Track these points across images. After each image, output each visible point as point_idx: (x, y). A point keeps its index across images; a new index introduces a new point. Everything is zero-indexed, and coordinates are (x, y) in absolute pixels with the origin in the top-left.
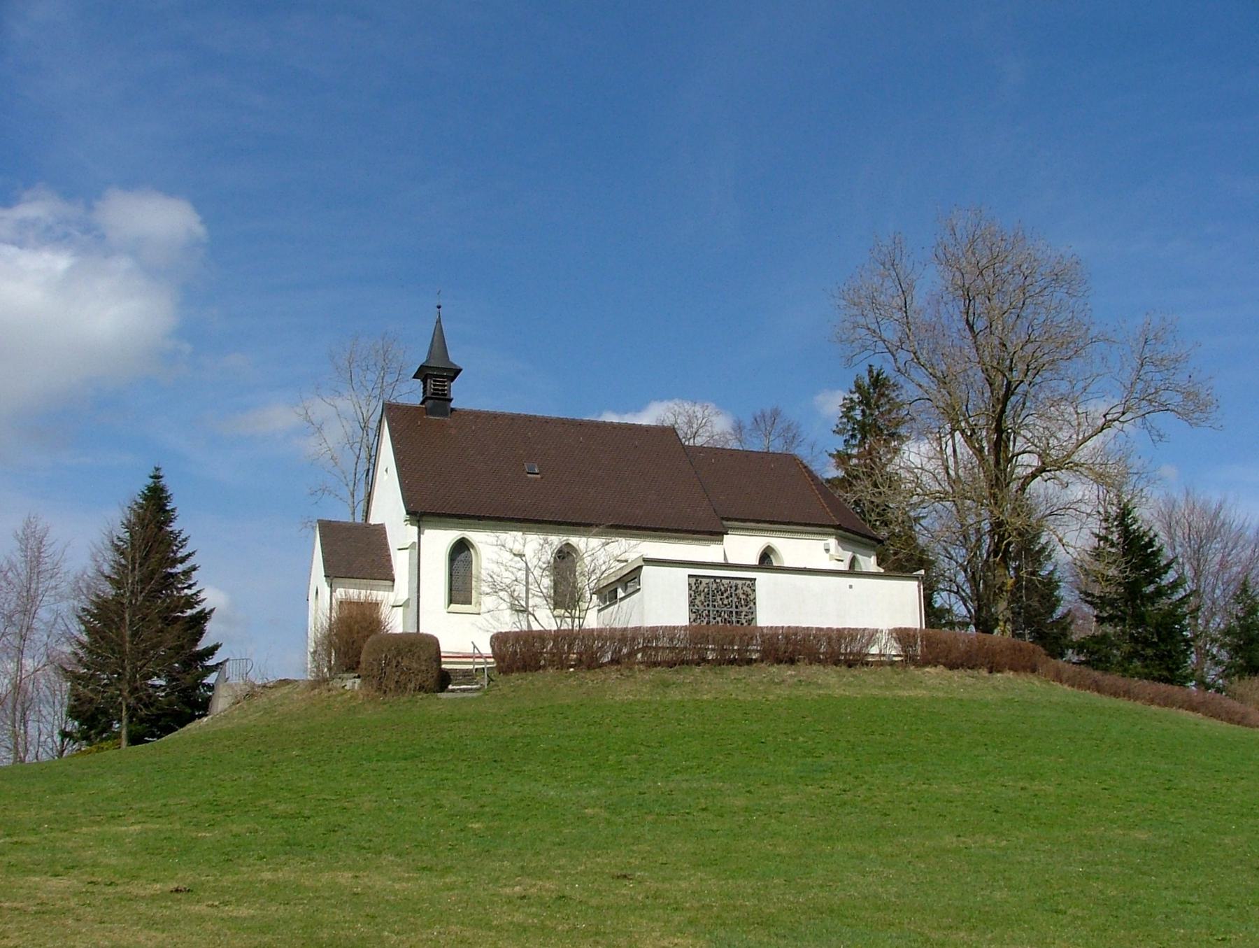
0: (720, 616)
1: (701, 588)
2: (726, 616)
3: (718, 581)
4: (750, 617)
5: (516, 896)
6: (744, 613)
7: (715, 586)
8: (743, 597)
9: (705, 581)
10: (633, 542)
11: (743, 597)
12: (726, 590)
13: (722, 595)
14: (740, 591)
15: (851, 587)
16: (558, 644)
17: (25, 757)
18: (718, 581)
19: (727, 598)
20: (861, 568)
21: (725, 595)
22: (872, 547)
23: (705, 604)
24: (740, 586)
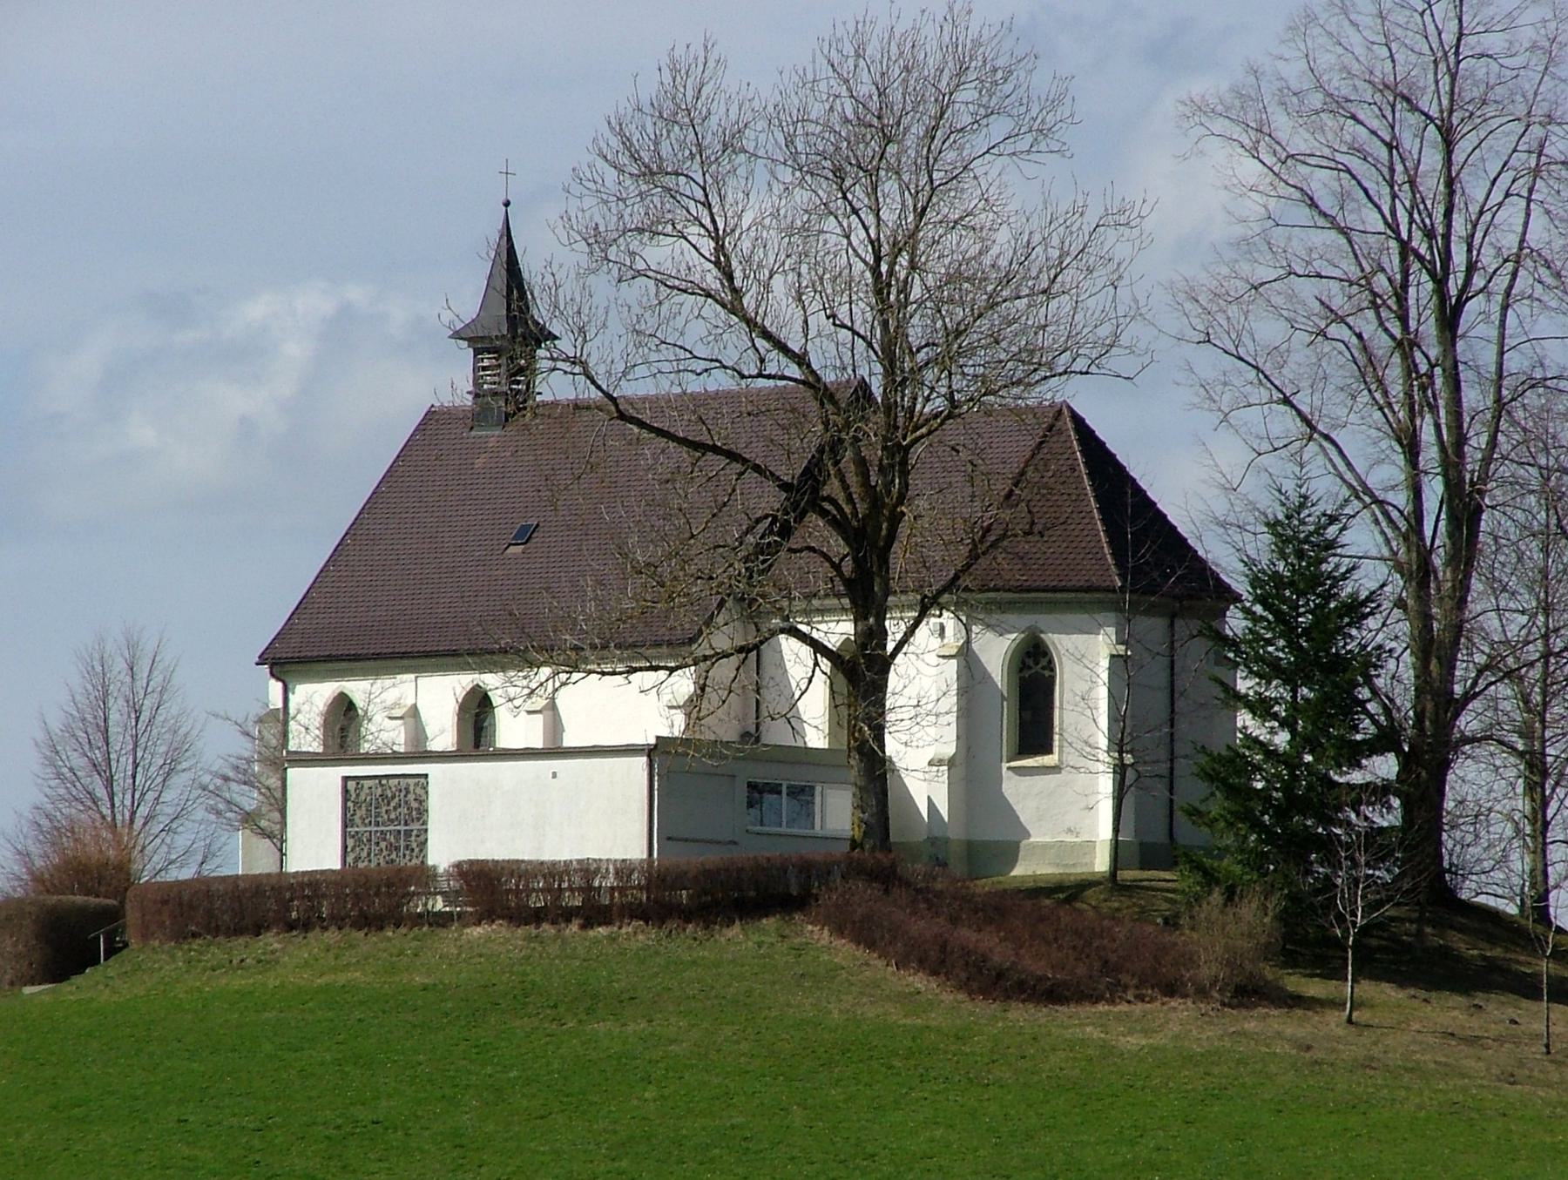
0: (385, 840)
1: (362, 797)
2: (392, 840)
3: (384, 782)
4: (422, 838)
5: (252, 718)
6: (415, 833)
7: (379, 791)
8: (415, 805)
9: (367, 783)
10: (386, 682)
11: (415, 805)
12: (393, 797)
13: (389, 804)
14: (411, 797)
15: (554, 775)
16: (812, 487)
17: (1538, 660)
18: (384, 782)
19: (395, 808)
20: (796, 732)
21: (393, 804)
22: (1102, 606)
23: (367, 821)
24: (411, 788)
